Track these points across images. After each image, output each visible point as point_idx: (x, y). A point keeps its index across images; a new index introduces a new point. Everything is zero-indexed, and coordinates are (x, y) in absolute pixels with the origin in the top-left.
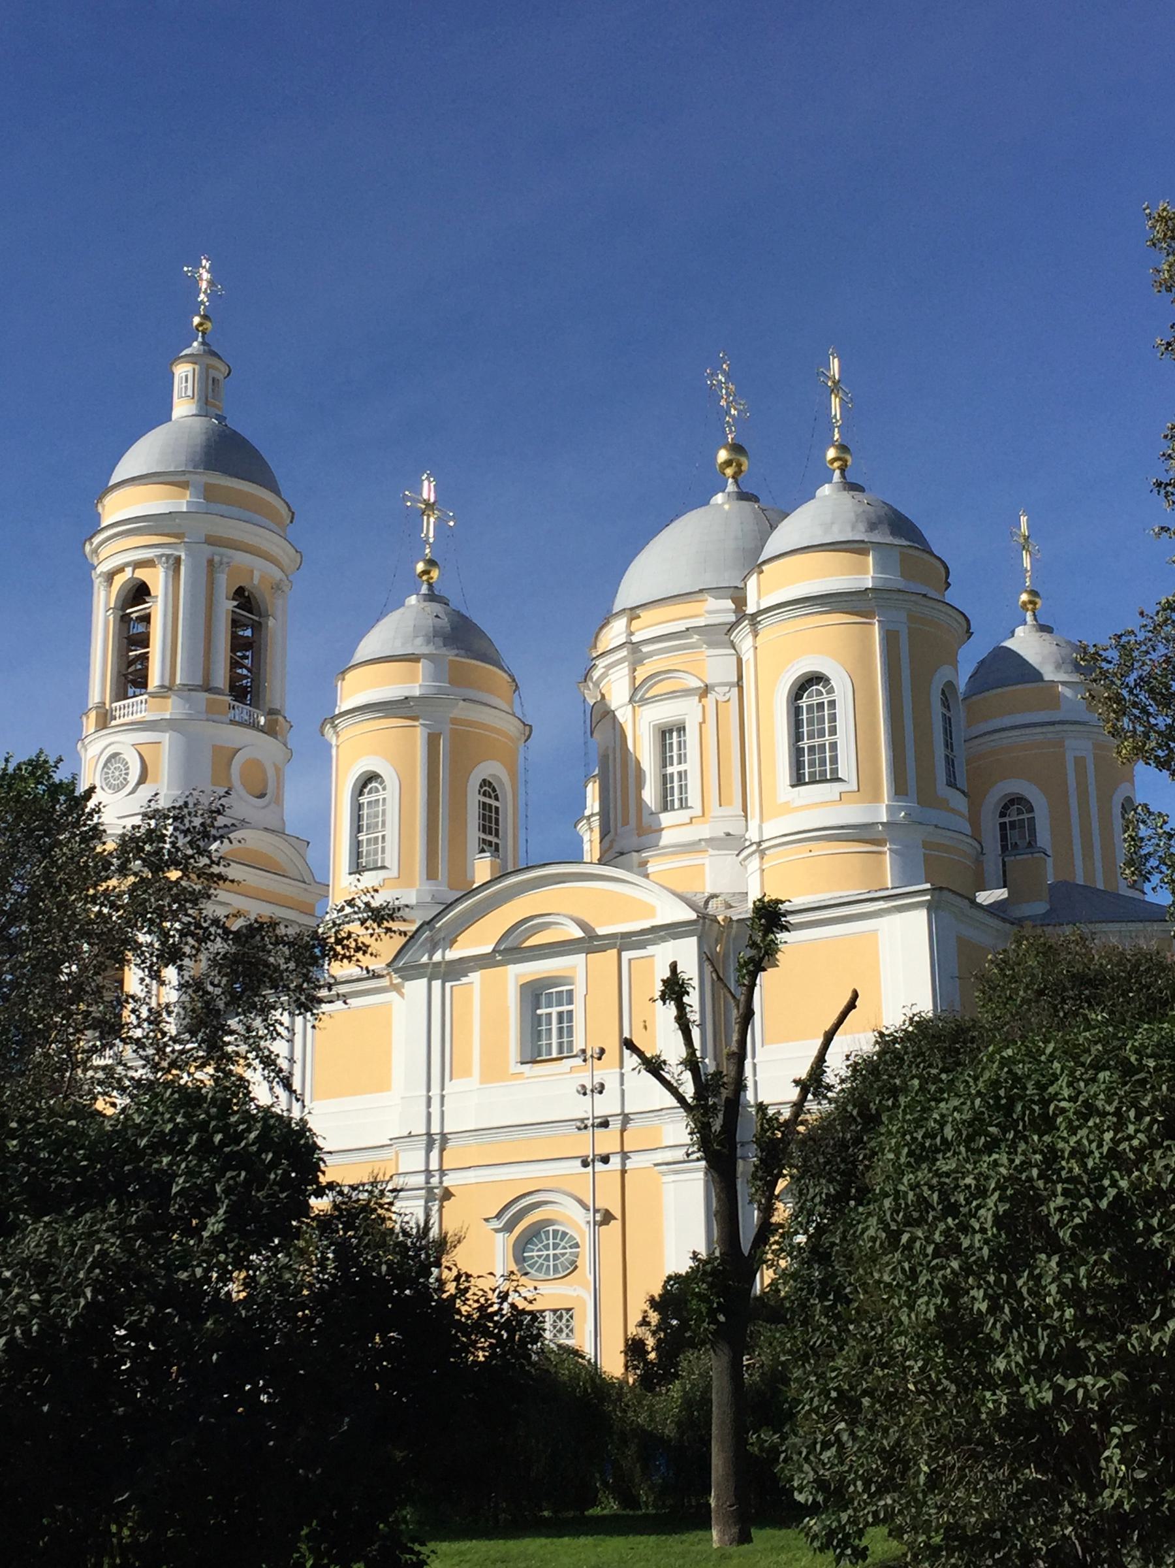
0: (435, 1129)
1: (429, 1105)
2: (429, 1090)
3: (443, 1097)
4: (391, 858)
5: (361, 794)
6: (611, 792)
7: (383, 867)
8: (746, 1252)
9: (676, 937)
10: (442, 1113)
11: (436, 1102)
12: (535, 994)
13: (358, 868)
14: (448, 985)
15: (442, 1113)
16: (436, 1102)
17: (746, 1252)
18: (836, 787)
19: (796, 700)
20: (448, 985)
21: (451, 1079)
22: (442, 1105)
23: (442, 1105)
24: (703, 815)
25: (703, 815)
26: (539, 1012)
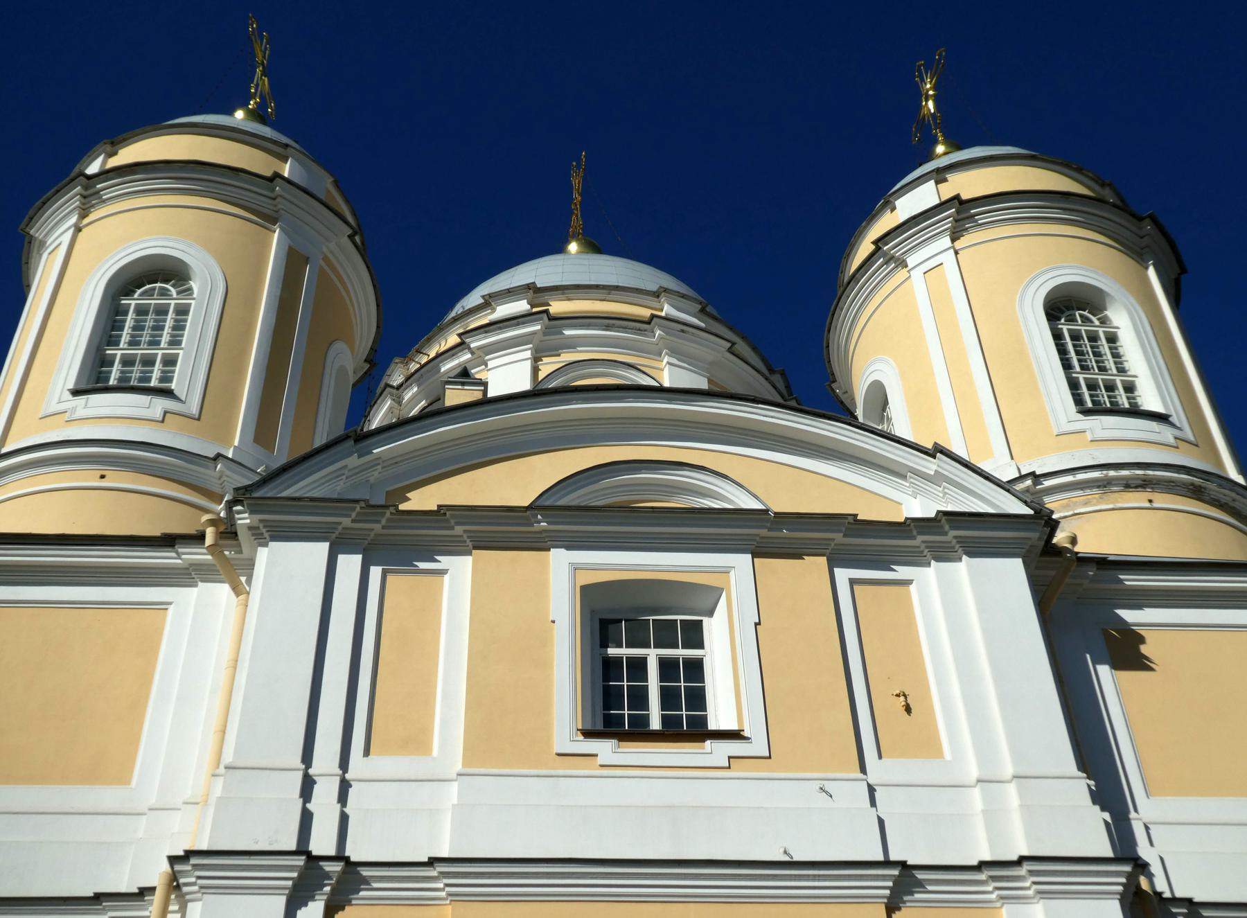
0: (322, 844)
1: (308, 786)
2: (307, 757)
3: (345, 786)
4: (188, 378)
5: (129, 293)
6: (1051, 419)
7: (168, 393)
8: (1032, 512)
9: (977, 550)
10: (344, 819)
11: (326, 792)
12: (610, 619)
13: (93, 380)
14: (376, 572)
15: (344, 819)
16: (326, 792)
17: (1032, 512)
18: (159, 405)
19: (604, 645)
20: (376, 572)
21: (367, 752)
22: (343, 798)
23: (343, 798)
24: (163, 421)
25: (163, 421)
26: (612, 651)
